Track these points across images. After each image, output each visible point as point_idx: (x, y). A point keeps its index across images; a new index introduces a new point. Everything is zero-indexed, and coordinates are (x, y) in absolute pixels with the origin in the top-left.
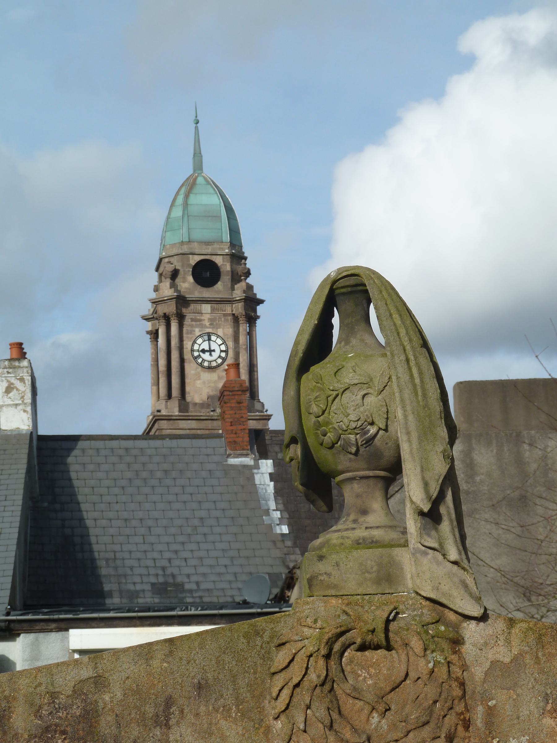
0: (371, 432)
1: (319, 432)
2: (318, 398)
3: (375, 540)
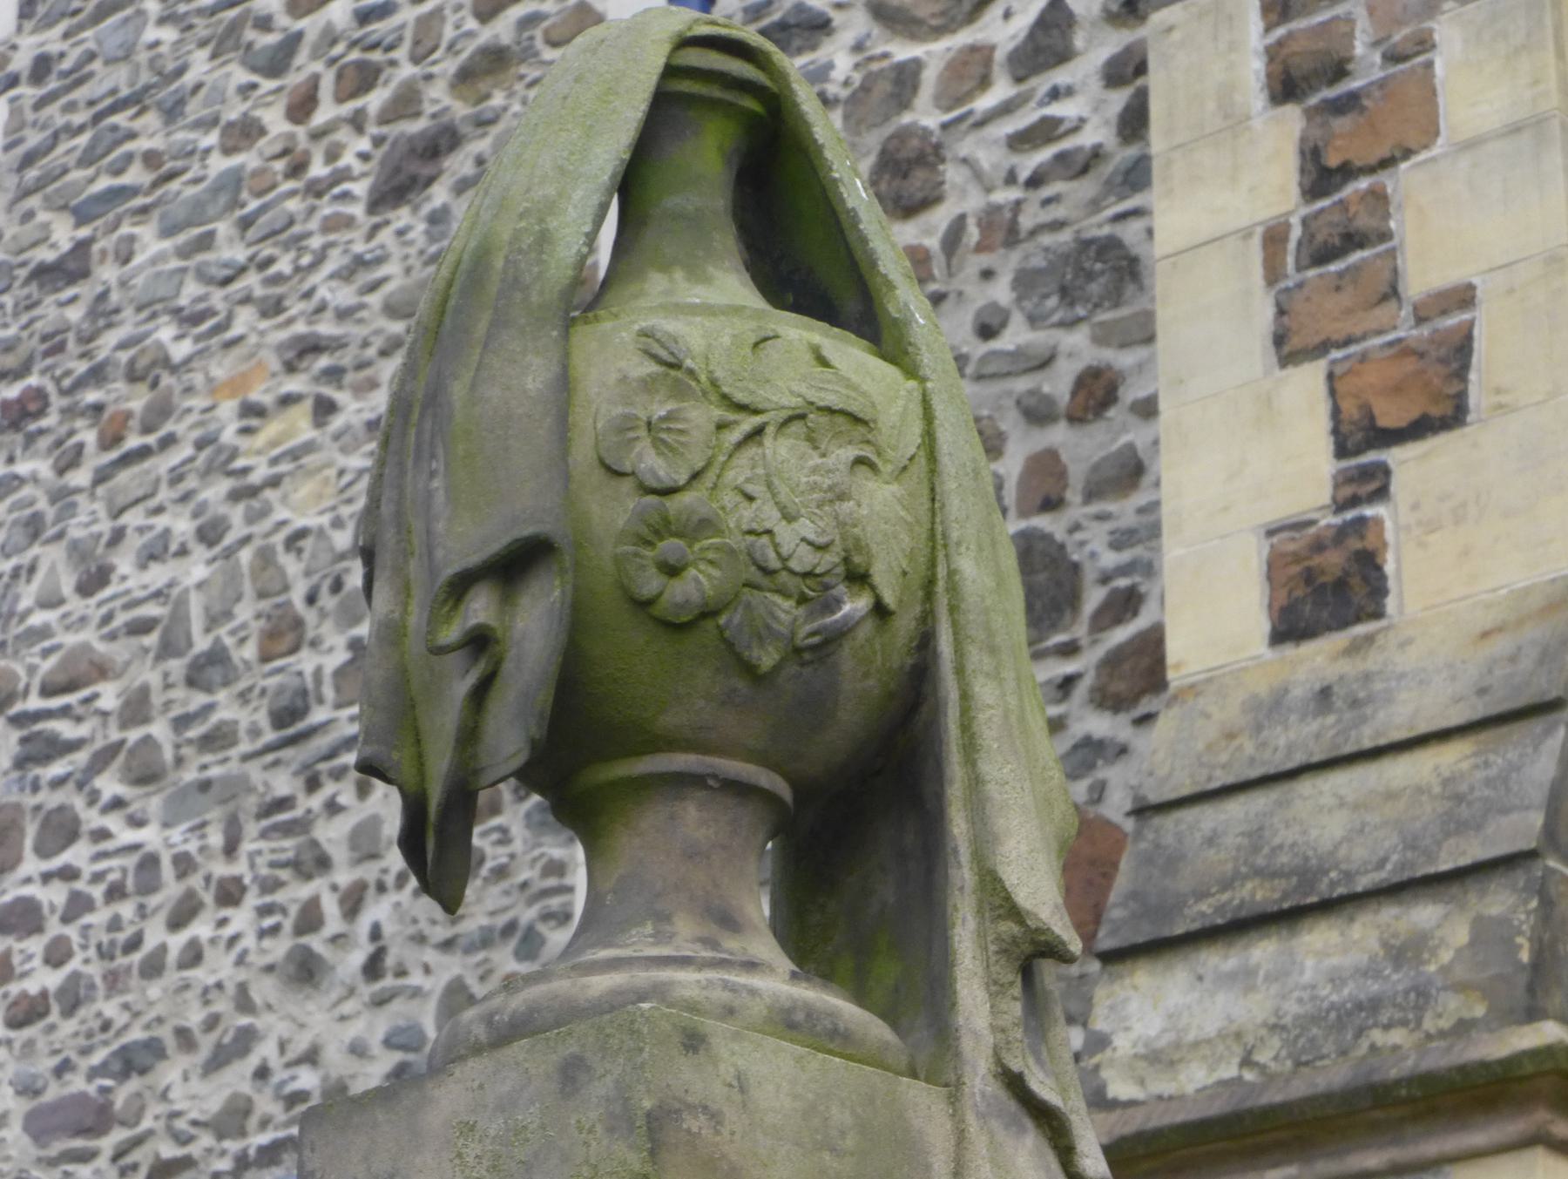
0: (847, 608)
1: (648, 553)
2: (677, 420)
3: (841, 1026)
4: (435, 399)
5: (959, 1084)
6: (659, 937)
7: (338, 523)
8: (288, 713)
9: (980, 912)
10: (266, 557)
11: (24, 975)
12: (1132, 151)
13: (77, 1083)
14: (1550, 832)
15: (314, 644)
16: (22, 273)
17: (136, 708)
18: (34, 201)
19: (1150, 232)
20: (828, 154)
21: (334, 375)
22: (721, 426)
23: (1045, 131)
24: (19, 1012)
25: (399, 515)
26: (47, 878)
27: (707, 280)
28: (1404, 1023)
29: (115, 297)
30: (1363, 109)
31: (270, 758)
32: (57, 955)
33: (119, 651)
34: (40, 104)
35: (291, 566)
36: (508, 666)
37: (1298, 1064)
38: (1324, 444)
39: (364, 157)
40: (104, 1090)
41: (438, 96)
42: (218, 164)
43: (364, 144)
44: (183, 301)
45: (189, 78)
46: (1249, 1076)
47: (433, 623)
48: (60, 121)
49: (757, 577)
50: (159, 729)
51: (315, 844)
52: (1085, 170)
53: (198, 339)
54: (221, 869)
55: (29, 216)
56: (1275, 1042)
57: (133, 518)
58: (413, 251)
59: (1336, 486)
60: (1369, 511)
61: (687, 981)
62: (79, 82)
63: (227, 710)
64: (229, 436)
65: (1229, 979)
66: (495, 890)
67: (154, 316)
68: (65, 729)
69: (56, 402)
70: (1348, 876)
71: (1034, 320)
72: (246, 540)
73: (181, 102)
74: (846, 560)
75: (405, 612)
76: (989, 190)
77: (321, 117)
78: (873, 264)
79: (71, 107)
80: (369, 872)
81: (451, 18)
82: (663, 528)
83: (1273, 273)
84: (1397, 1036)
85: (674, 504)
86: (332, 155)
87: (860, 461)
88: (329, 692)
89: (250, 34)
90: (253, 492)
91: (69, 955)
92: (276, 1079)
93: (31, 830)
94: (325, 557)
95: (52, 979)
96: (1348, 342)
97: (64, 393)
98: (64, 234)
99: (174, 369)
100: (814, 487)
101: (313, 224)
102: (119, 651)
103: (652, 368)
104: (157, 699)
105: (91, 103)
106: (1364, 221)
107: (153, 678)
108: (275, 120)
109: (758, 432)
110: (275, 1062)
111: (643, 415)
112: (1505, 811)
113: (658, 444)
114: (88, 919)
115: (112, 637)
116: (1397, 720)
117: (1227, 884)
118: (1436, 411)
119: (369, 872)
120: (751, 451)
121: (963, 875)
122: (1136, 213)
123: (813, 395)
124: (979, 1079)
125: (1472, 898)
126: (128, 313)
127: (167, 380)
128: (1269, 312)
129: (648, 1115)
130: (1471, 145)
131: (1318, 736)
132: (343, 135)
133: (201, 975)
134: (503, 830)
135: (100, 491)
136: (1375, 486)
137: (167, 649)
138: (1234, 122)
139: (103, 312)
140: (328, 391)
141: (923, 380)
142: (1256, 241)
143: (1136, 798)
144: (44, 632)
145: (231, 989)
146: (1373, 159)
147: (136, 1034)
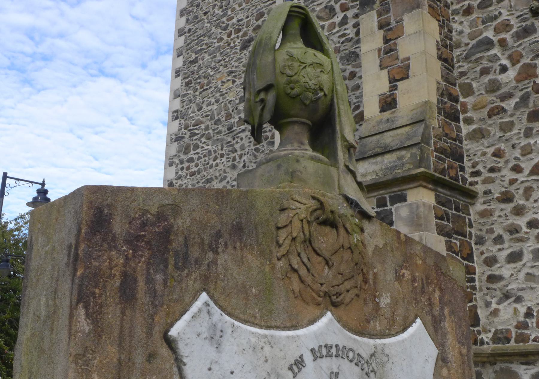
0: (320, 94)
4: (254, 63)
5: (339, 167)
6: (291, 146)
7: (237, 99)
8: (230, 128)
9: (341, 141)
10: (226, 104)
11: (192, 169)
12: (357, 38)
13: (200, 184)
14: (422, 140)
15: (233, 118)
16: (188, 62)
17: (207, 128)
18: (189, 51)
19: (360, 50)
20: (315, 24)
21: (235, 76)
22: (300, 66)
23: (344, 35)
24: (191, 174)
25: (249, 82)
26: (195, 154)
27: (296, 44)
28: (400, 169)
29: (202, 65)
30: (393, 30)
31: (227, 135)
32: (197, 166)
33: (204, 119)
34: (189, 37)
35: (229, 106)
36: (267, 104)
37: (384, 175)
38: (388, 82)
39: (239, 43)
40: (204, 185)
41: (250, 33)
42: (217, 44)
43: (239, 41)
44: (212, 66)
45: (212, 31)
46: (377, 177)
47: (255, 98)
48: (193, 39)
49: (306, 89)
50: (211, 131)
51: (235, 148)
52: (350, 41)
53: (214, 72)
54: (221, 152)
55: (188, 53)
56: (381, 172)
57: (205, 99)
58: (247, 57)
59: (389, 88)
60: (394, 92)
61: (296, 152)
62: (196, 32)
63: (221, 128)
64: (219, 86)
65: (374, 163)
66: (262, 154)
67: (208, 68)
68: (196, 131)
69: (193, 82)
70: (392, 147)
71: (343, 64)
72: (223, 102)
73: (211, 35)
74: (320, 87)
75: (250, 97)
76: (335, 44)
77: (232, 37)
78: (323, 41)
79: (194, 37)
80: (243, 152)
81: (252, 21)
82: (290, 82)
83: (379, 56)
84: (399, 171)
85: (292, 78)
86: (234, 43)
87: (321, 71)
88: (236, 125)
89: (221, 24)
90: (223, 95)
91: (198, 165)
92: (230, 183)
93: (192, 147)
94: (235, 104)
95: (196, 169)
96: (391, 66)
97: (194, 80)
98: (194, 56)
99: (211, 76)
100: (314, 75)
101: (231, 53)
102: (204, 119)
103: (288, 57)
104: (210, 127)
105: (197, 36)
106: (393, 48)
107: (209, 123)
108: (225, 37)
109: (305, 67)
110: (230, 181)
111: (287, 64)
112: (415, 137)
113: (290, 69)
114: (201, 160)
115: (203, 117)
116: (398, 124)
117: (373, 149)
118: (404, 76)
119: (243, 152)
120: (304, 70)
121: (339, 135)
122: (358, 47)
123: (314, 61)
124: (342, 166)
125: (410, 150)
126: (204, 68)
127: (210, 78)
128: (379, 62)
129: (291, 172)
130: (409, 35)
131: (387, 126)
132: (236, 39)
133: (218, 168)
134: (263, 145)
135: (200, 95)
136: (395, 88)
137: (211, 119)
138: (373, 33)
139: (200, 68)
140: (234, 79)
141: (331, 59)
142: (377, 51)
143: (360, 137)
144: (193, 117)
145: (223, 170)
146: (395, 38)
147: (209, 177)
